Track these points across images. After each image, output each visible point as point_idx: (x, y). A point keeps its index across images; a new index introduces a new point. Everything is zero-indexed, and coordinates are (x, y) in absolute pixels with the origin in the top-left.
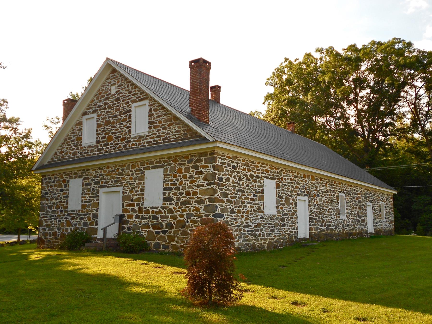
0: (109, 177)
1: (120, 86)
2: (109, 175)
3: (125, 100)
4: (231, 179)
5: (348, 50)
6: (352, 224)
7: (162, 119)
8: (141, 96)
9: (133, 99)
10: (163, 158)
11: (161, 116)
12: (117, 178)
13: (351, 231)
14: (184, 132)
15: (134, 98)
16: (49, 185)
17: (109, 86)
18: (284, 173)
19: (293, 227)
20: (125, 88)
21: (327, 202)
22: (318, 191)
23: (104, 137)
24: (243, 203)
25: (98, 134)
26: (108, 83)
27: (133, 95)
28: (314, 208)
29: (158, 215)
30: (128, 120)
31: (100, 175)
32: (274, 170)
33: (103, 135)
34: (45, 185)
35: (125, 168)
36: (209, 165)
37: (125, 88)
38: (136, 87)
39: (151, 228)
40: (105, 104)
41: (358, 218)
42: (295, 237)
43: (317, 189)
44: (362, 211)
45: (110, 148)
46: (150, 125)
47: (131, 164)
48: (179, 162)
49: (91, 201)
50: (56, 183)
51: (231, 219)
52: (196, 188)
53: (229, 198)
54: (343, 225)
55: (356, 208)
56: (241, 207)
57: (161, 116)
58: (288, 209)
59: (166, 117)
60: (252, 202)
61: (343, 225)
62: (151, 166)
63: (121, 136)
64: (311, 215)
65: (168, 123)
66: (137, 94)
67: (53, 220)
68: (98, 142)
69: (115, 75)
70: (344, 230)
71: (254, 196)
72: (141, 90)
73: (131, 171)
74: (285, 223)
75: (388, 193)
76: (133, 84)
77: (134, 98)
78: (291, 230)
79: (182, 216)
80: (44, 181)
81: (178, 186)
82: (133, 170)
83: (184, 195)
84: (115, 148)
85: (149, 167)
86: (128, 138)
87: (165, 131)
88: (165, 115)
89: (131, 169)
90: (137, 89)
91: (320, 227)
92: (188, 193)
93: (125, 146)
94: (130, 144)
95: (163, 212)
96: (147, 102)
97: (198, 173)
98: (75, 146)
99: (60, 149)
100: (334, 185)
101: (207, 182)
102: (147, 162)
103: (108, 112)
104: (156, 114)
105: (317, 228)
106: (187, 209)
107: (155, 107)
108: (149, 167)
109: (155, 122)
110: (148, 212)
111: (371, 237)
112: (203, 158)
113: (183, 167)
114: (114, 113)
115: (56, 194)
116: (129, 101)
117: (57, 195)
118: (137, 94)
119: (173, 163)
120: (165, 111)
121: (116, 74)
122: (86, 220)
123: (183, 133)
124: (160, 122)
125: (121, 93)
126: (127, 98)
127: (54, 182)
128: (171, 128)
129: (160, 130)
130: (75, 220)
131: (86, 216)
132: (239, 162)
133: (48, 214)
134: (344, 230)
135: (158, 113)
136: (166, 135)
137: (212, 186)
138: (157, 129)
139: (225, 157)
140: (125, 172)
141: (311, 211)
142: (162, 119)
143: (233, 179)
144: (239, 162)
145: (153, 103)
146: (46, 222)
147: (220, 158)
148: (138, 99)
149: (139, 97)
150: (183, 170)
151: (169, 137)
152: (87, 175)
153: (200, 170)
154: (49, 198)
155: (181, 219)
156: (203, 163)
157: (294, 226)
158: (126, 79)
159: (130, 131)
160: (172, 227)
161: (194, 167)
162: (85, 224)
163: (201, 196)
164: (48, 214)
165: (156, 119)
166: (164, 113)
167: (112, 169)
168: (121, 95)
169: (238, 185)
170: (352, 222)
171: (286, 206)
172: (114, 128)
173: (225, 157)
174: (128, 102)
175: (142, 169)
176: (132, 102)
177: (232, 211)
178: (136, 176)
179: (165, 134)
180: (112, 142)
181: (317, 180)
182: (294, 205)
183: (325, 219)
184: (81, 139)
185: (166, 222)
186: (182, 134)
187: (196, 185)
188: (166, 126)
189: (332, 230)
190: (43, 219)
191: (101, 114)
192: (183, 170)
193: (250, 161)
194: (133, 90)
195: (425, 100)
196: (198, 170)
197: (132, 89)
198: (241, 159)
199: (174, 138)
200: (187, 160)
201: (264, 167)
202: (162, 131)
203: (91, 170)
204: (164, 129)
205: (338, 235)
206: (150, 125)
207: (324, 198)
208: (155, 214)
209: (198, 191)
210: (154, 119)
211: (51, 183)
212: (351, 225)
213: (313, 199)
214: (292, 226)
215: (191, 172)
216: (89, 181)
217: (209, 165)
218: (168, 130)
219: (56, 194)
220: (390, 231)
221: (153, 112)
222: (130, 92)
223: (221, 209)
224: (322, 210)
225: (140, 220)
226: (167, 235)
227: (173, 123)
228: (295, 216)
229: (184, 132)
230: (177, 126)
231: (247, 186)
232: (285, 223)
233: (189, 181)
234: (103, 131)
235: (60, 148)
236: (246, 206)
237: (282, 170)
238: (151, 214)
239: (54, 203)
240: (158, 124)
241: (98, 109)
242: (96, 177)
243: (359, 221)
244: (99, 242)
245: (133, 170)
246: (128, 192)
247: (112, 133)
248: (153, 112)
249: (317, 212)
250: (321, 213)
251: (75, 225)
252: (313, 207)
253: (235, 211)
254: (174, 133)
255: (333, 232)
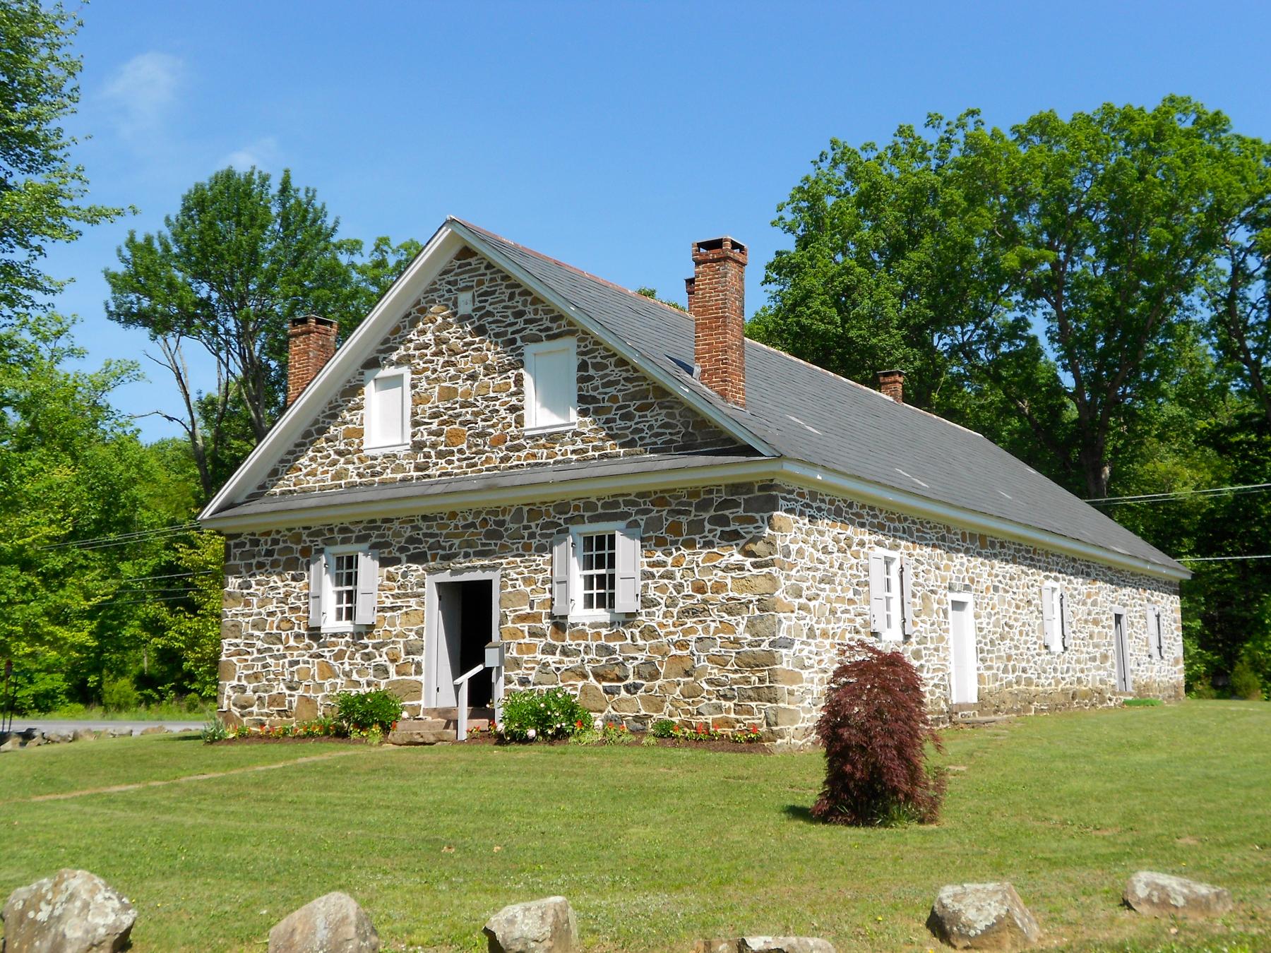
0: (457, 542)
1: (486, 294)
2: (456, 536)
3: (505, 333)
4: (808, 550)
5: (1022, 135)
6: (1078, 667)
7: (620, 391)
8: (555, 325)
9: (528, 332)
10: (623, 495)
11: (617, 382)
12: (483, 545)
13: (1076, 686)
14: (687, 428)
15: (532, 329)
16: (254, 561)
17: (449, 291)
18: (918, 530)
19: (940, 674)
20: (503, 301)
21: (1018, 607)
22: (997, 576)
23: (438, 433)
24: (833, 612)
25: (416, 424)
26: (449, 283)
27: (526, 322)
28: (988, 624)
29: (612, 644)
30: (513, 389)
31: (425, 535)
32: (897, 524)
33: (434, 427)
34: (238, 562)
35: (507, 518)
36: (757, 516)
37: (503, 301)
38: (537, 301)
39: (591, 678)
40: (439, 341)
41: (1091, 649)
42: (946, 701)
43: (994, 572)
44: (1100, 628)
45: (457, 463)
46: (585, 406)
47: (526, 509)
48: (673, 507)
49: (400, 608)
50: (276, 556)
51: (810, 652)
52: (720, 573)
53: (803, 600)
54: (1055, 670)
55: (1086, 621)
56: (828, 622)
57: (617, 382)
58: (928, 626)
59: (630, 386)
60: (850, 608)
61: (1055, 670)
62: (587, 514)
63: (491, 430)
64: (980, 642)
65: (638, 403)
66: (541, 319)
67: (269, 660)
68: (418, 446)
69: (470, 264)
70: (1058, 683)
71: (856, 592)
72: (552, 311)
73: (526, 528)
74: (922, 662)
75: (1168, 579)
76: (527, 293)
77: (532, 329)
78: (936, 681)
79: (682, 645)
80: (233, 551)
81: (669, 568)
82: (533, 524)
83: (688, 590)
84: (475, 465)
85: (583, 516)
86: (513, 438)
87: (629, 424)
88: (626, 379)
89: (525, 522)
90: (540, 307)
91: (1001, 675)
92: (700, 589)
93: (505, 459)
94: (523, 454)
95: (629, 636)
96: (570, 344)
97: (726, 536)
98: (340, 453)
99: (288, 461)
100: (1032, 559)
101: (753, 560)
102: (576, 502)
103: (448, 364)
104: (602, 377)
105: (995, 675)
106: (699, 627)
107: (599, 360)
108: (583, 516)
109: (600, 397)
110: (582, 635)
111: (1126, 702)
112: (741, 499)
113: (683, 519)
114: (468, 369)
115: (277, 588)
116: (517, 336)
117: (282, 591)
118: (541, 319)
119: (656, 509)
120: (628, 371)
121: (473, 260)
122: (382, 660)
123: (683, 430)
124: (614, 399)
125: (489, 314)
126: (510, 330)
127: (269, 553)
128: (646, 416)
129: (614, 420)
130: (346, 660)
131: (385, 650)
132: (823, 506)
133: (252, 645)
134: (1058, 683)
135: (607, 375)
136: (632, 433)
137: (766, 570)
138: (605, 417)
139: (794, 496)
140: (506, 530)
141: (981, 629)
142: (620, 391)
143: (811, 550)
144: (823, 506)
145: (590, 347)
146: (246, 667)
147: (784, 499)
148: (543, 334)
149: (548, 329)
150: (685, 527)
151: (641, 439)
152: (383, 536)
153: (732, 528)
154: (255, 600)
155: (679, 653)
156: (741, 511)
157: (943, 670)
158: (506, 278)
159: (519, 421)
160: (654, 676)
161: (713, 520)
162: (382, 671)
163: (737, 595)
164: (252, 645)
165: (601, 390)
166: (625, 375)
167: (465, 519)
168: (490, 319)
169: (821, 566)
170: (1078, 661)
171: (923, 617)
172: (470, 410)
173: (794, 496)
174: (513, 341)
175: (562, 522)
176: (523, 339)
177: (811, 633)
178: (543, 541)
179: (627, 432)
180: (464, 446)
181: (993, 545)
182: (942, 615)
183: (1013, 652)
184: (360, 433)
185: (636, 663)
186: (679, 433)
187: (723, 566)
188: (632, 409)
189: (1029, 682)
190: (234, 659)
191: (426, 369)
192: (685, 527)
193: (845, 501)
194: (529, 308)
195: (1256, 291)
196: (727, 529)
197: (525, 304)
198: (827, 499)
199: (655, 443)
200: (695, 501)
201: (875, 516)
202: (618, 422)
203: (396, 523)
204: (627, 417)
205: (1047, 696)
206: (585, 406)
207: (1009, 596)
208: (603, 642)
209: (729, 581)
210: (596, 389)
211: (260, 555)
212: (1074, 670)
213: (983, 598)
214: (939, 670)
215: (706, 533)
216: (390, 552)
217: (757, 516)
218: (637, 420)
219: (277, 588)
220: (1175, 687)
221: (591, 372)
222: (519, 314)
223: (789, 627)
224: (1007, 629)
225: (557, 657)
226: (641, 698)
227: (652, 404)
228: (943, 644)
229: (687, 428)
230: (664, 412)
231: (840, 567)
232: (922, 662)
233: (702, 556)
234: (435, 415)
235: (289, 457)
236: (839, 620)
237: (914, 522)
238: (589, 642)
239: (271, 614)
240: (606, 404)
241: (417, 353)
242: (411, 540)
243: (1094, 659)
244: (429, 719)
245: (533, 524)
246: (520, 582)
247: (463, 424)
248: (591, 372)
249: (995, 633)
250: (1002, 638)
251: (347, 674)
252: (984, 620)
253: (818, 632)
254: (656, 430)
255: (1033, 688)
